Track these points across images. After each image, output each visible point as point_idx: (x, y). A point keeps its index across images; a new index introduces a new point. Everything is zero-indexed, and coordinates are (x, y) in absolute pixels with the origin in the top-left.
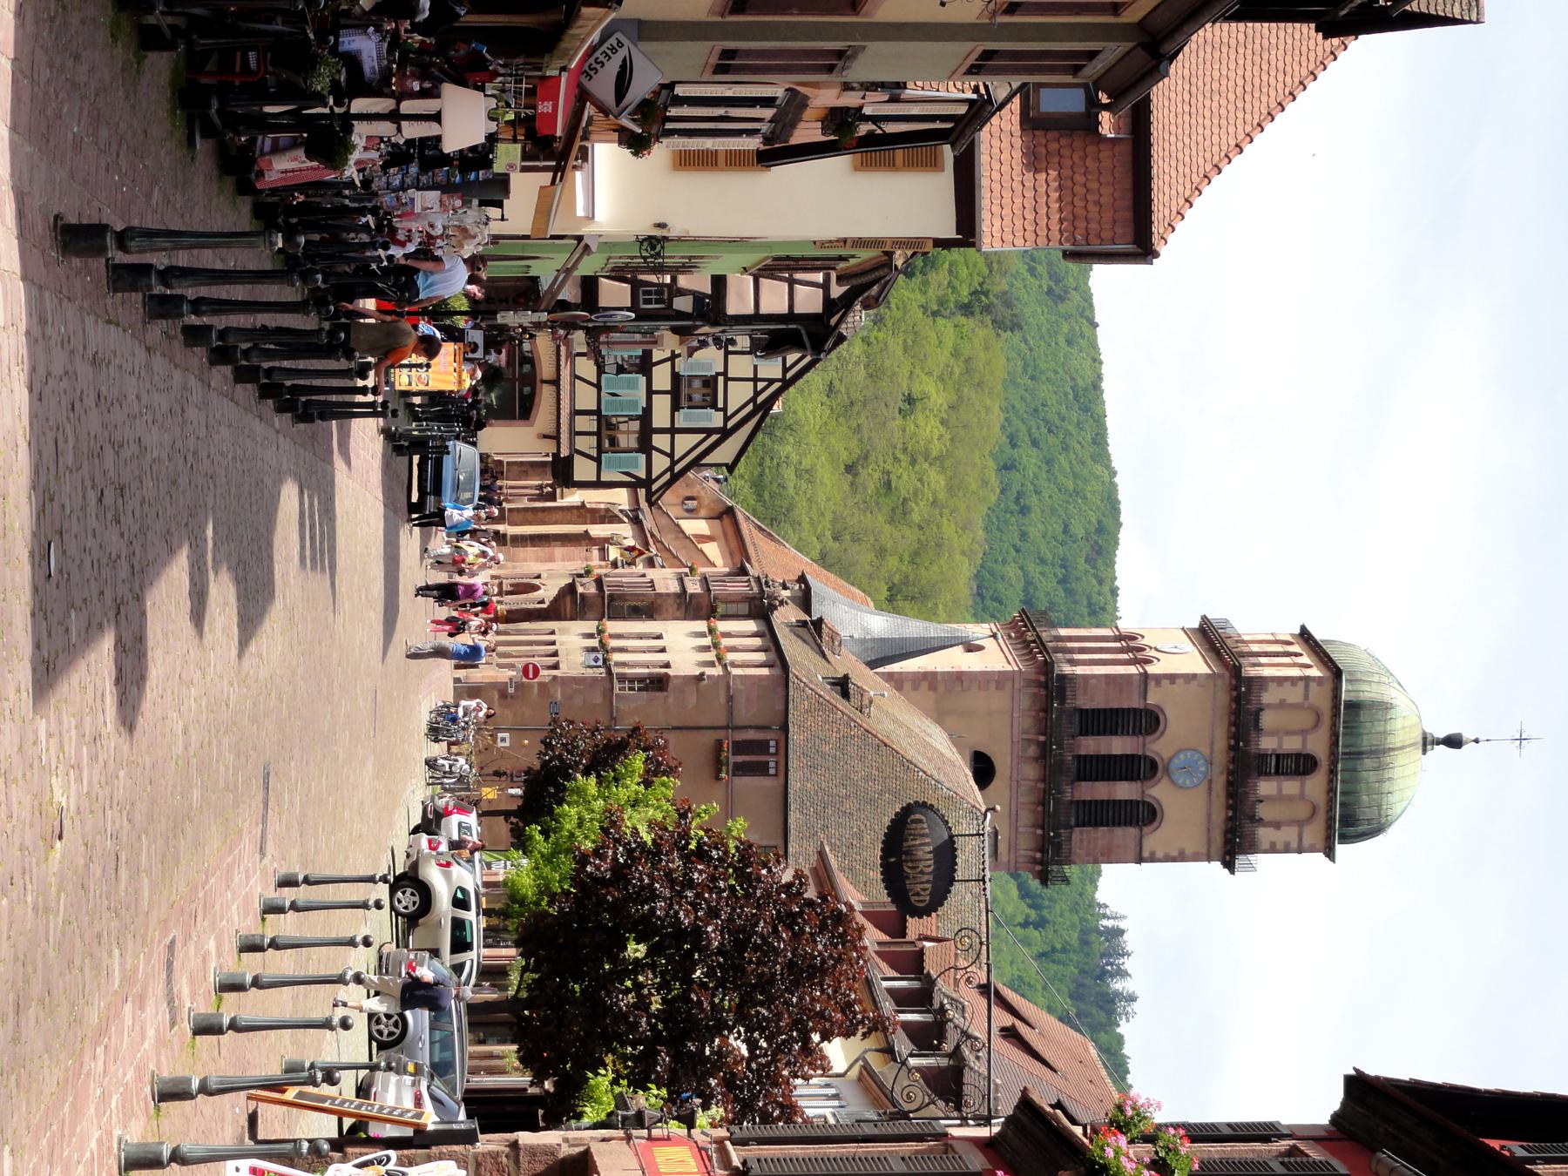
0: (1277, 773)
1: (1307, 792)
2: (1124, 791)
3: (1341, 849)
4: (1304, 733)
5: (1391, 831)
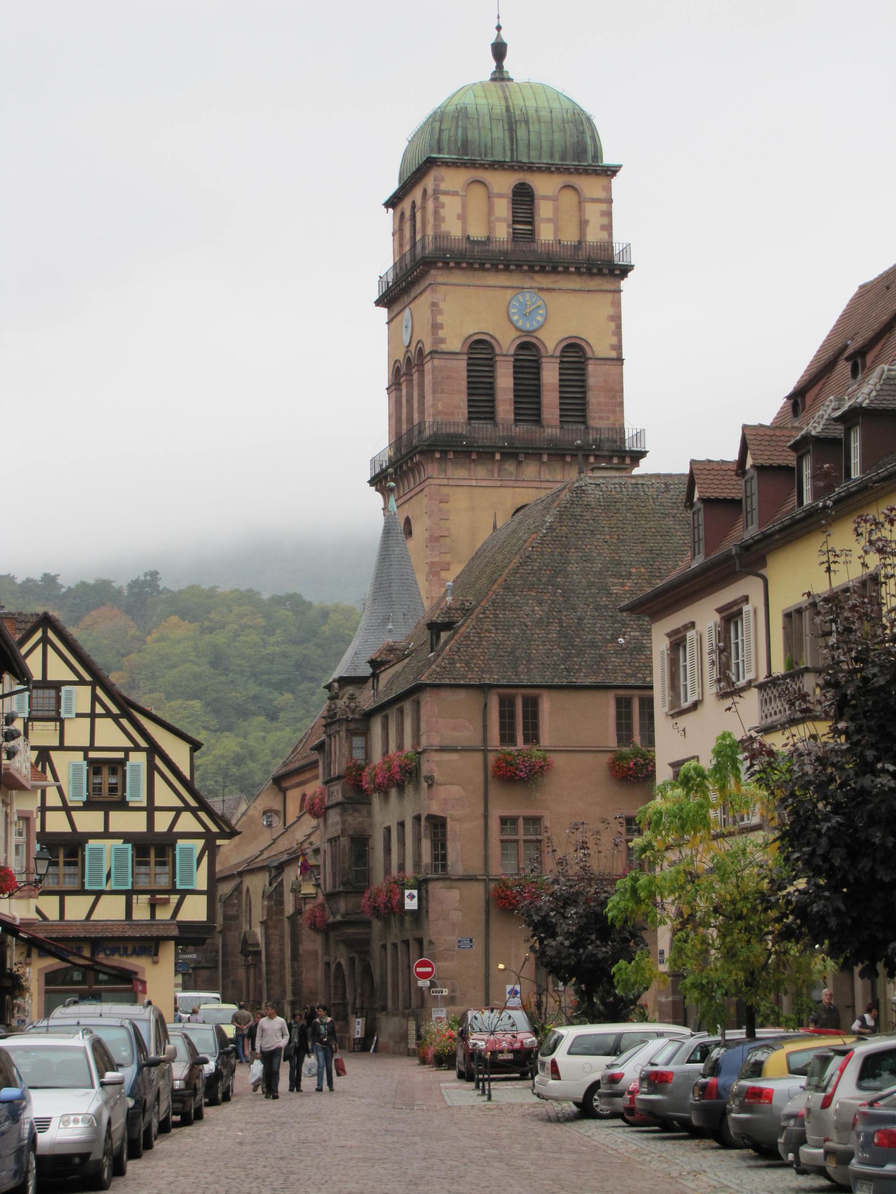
0: (531, 223)
1: (550, 194)
2: (550, 375)
3: (608, 159)
4: (490, 197)
5: (588, 107)
